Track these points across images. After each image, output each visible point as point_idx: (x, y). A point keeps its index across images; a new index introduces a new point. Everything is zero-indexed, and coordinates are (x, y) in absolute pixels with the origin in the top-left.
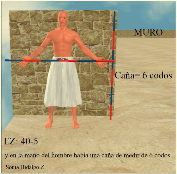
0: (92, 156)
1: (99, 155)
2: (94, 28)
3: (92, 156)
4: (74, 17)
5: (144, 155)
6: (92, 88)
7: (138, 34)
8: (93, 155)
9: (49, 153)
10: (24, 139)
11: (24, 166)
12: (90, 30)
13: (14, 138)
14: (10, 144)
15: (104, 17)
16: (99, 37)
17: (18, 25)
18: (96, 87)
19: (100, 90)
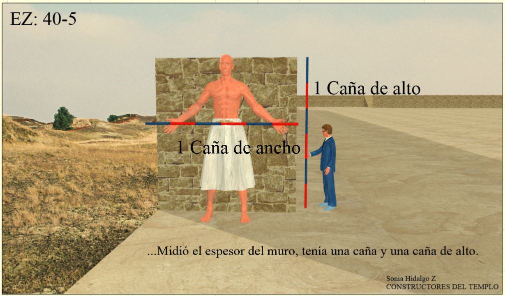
0: (394, 253)
1: (348, 250)
2: (266, 83)
3: (394, 253)
4: (241, 67)
5: (446, 251)
6: (266, 171)
7: (162, 254)
8: (337, 251)
9: (200, 247)
10: (49, 14)
11: (411, 277)
12: (261, 86)
13: (30, 13)
14: (23, 24)
15: (279, 67)
16: (274, 96)
17: (167, 78)
18: (271, 168)
19: (276, 172)
